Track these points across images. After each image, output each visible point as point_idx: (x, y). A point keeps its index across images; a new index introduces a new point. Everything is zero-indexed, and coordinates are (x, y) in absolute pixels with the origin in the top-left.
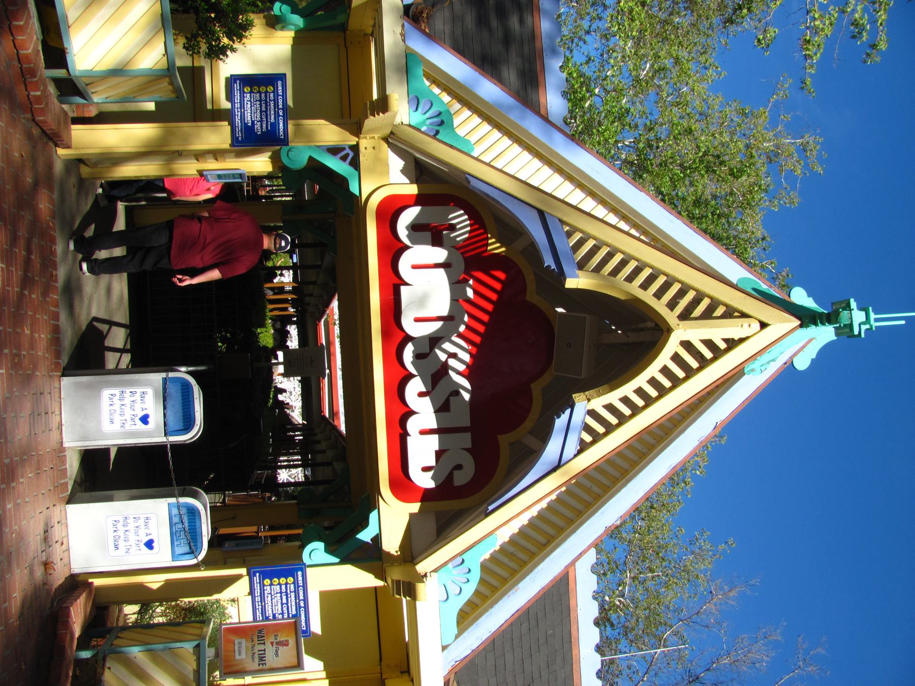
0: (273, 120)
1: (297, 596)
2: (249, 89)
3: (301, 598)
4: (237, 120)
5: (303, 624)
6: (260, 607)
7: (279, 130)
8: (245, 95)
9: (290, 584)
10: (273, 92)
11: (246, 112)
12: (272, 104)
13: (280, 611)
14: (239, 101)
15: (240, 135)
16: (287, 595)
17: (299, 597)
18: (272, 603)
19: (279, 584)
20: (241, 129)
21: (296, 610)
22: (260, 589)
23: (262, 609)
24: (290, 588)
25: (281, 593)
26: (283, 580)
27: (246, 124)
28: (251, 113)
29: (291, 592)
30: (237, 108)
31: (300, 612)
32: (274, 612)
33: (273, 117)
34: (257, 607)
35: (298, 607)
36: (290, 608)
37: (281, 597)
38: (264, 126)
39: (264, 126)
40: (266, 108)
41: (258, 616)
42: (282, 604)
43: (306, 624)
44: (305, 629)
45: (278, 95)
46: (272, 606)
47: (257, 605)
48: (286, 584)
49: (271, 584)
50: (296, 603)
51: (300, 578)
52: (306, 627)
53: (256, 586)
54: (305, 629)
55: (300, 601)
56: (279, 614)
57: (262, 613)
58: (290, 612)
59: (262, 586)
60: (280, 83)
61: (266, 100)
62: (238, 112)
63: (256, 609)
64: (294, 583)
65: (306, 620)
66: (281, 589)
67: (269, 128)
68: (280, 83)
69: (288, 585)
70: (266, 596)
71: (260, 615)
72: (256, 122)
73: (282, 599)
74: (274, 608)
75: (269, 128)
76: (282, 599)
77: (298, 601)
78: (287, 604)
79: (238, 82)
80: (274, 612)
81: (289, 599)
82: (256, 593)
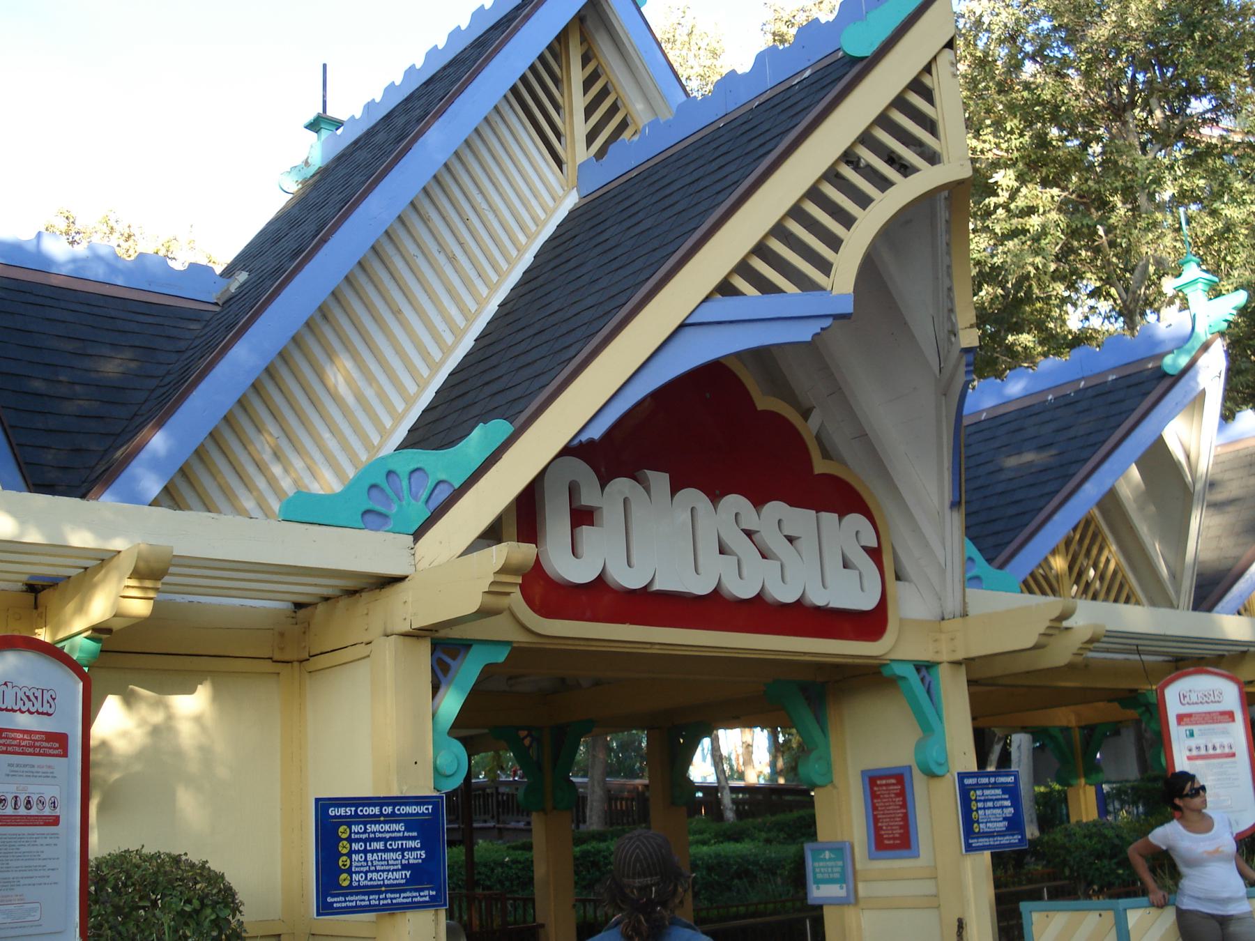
0: (401, 827)
1: (374, 819)
2: (344, 876)
3: (376, 810)
4: (401, 900)
5: (423, 809)
6: (389, 895)
7: (417, 814)
8: (355, 884)
9: (351, 833)
10: (349, 825)
11: (386, 882)
12: (987, 792)
13: (398, 855)
14: (366, 898)
15: (426, 893)
16: (371, 840)
17: (375, 816)
18: (383, 871)
19: (349, 855)
20: (416, 890)
21: (397, 822)
22: (357, 894)
23: (392, 892)
24: (358, 833)
25: (365, 852)
26: (344, 848)
27: (409, 881)
28: (388, 871)
29: (365, 832)
30: (379, 899)
31: (401, 815)
32: (400, 867)
33: (395, 827)
34: (389, 901)
35: (392, 819)
36: (393, 835)
37: (373, 852)
38: (411, 844)
39: (411, 844)
40: (990, 800)
41: (405, 900)
42: (386, 850)
43: (424, 804)
44: (430, 807)
45: (977, 784)
46: (388, 871)
47: (385, 902)
48: (350, 840)
49: (349, 871)
50: (385, 822)
51: (342, 811)
52: (428, 803)
53: (351, 904)
54: (430, 807)
55: (381, 814)
56: (403, 856)
57: (400, 892)
58: (401, 834)
59: (352, 890)
60: (332, 812)
61: (365, 841)
62: (386, 898)
63: (392, 904)
64: (349, 825)
65: (417, 804)
66: (358, 852)
67: (415, 834)
68: (332, 812)
69: (978, 798)
70: (369, 883)
71: (402, 895)
72: (404, 862)
73: (377, 851)
74: (392, 868)
75: (415, 834)
76: (377, 851)
77: (382, 819)
78: (385, 840)
79: (329, 900)
80: (400, 867)
81: (378, 835)
82: (363, 903)
